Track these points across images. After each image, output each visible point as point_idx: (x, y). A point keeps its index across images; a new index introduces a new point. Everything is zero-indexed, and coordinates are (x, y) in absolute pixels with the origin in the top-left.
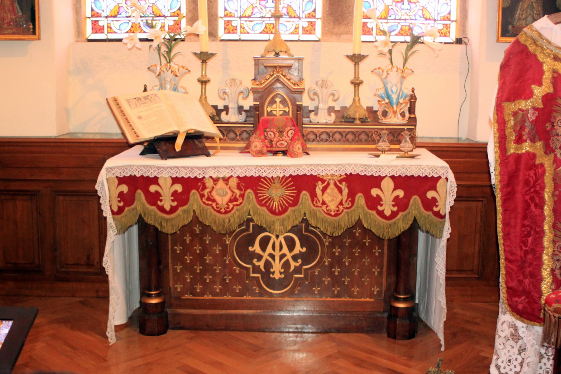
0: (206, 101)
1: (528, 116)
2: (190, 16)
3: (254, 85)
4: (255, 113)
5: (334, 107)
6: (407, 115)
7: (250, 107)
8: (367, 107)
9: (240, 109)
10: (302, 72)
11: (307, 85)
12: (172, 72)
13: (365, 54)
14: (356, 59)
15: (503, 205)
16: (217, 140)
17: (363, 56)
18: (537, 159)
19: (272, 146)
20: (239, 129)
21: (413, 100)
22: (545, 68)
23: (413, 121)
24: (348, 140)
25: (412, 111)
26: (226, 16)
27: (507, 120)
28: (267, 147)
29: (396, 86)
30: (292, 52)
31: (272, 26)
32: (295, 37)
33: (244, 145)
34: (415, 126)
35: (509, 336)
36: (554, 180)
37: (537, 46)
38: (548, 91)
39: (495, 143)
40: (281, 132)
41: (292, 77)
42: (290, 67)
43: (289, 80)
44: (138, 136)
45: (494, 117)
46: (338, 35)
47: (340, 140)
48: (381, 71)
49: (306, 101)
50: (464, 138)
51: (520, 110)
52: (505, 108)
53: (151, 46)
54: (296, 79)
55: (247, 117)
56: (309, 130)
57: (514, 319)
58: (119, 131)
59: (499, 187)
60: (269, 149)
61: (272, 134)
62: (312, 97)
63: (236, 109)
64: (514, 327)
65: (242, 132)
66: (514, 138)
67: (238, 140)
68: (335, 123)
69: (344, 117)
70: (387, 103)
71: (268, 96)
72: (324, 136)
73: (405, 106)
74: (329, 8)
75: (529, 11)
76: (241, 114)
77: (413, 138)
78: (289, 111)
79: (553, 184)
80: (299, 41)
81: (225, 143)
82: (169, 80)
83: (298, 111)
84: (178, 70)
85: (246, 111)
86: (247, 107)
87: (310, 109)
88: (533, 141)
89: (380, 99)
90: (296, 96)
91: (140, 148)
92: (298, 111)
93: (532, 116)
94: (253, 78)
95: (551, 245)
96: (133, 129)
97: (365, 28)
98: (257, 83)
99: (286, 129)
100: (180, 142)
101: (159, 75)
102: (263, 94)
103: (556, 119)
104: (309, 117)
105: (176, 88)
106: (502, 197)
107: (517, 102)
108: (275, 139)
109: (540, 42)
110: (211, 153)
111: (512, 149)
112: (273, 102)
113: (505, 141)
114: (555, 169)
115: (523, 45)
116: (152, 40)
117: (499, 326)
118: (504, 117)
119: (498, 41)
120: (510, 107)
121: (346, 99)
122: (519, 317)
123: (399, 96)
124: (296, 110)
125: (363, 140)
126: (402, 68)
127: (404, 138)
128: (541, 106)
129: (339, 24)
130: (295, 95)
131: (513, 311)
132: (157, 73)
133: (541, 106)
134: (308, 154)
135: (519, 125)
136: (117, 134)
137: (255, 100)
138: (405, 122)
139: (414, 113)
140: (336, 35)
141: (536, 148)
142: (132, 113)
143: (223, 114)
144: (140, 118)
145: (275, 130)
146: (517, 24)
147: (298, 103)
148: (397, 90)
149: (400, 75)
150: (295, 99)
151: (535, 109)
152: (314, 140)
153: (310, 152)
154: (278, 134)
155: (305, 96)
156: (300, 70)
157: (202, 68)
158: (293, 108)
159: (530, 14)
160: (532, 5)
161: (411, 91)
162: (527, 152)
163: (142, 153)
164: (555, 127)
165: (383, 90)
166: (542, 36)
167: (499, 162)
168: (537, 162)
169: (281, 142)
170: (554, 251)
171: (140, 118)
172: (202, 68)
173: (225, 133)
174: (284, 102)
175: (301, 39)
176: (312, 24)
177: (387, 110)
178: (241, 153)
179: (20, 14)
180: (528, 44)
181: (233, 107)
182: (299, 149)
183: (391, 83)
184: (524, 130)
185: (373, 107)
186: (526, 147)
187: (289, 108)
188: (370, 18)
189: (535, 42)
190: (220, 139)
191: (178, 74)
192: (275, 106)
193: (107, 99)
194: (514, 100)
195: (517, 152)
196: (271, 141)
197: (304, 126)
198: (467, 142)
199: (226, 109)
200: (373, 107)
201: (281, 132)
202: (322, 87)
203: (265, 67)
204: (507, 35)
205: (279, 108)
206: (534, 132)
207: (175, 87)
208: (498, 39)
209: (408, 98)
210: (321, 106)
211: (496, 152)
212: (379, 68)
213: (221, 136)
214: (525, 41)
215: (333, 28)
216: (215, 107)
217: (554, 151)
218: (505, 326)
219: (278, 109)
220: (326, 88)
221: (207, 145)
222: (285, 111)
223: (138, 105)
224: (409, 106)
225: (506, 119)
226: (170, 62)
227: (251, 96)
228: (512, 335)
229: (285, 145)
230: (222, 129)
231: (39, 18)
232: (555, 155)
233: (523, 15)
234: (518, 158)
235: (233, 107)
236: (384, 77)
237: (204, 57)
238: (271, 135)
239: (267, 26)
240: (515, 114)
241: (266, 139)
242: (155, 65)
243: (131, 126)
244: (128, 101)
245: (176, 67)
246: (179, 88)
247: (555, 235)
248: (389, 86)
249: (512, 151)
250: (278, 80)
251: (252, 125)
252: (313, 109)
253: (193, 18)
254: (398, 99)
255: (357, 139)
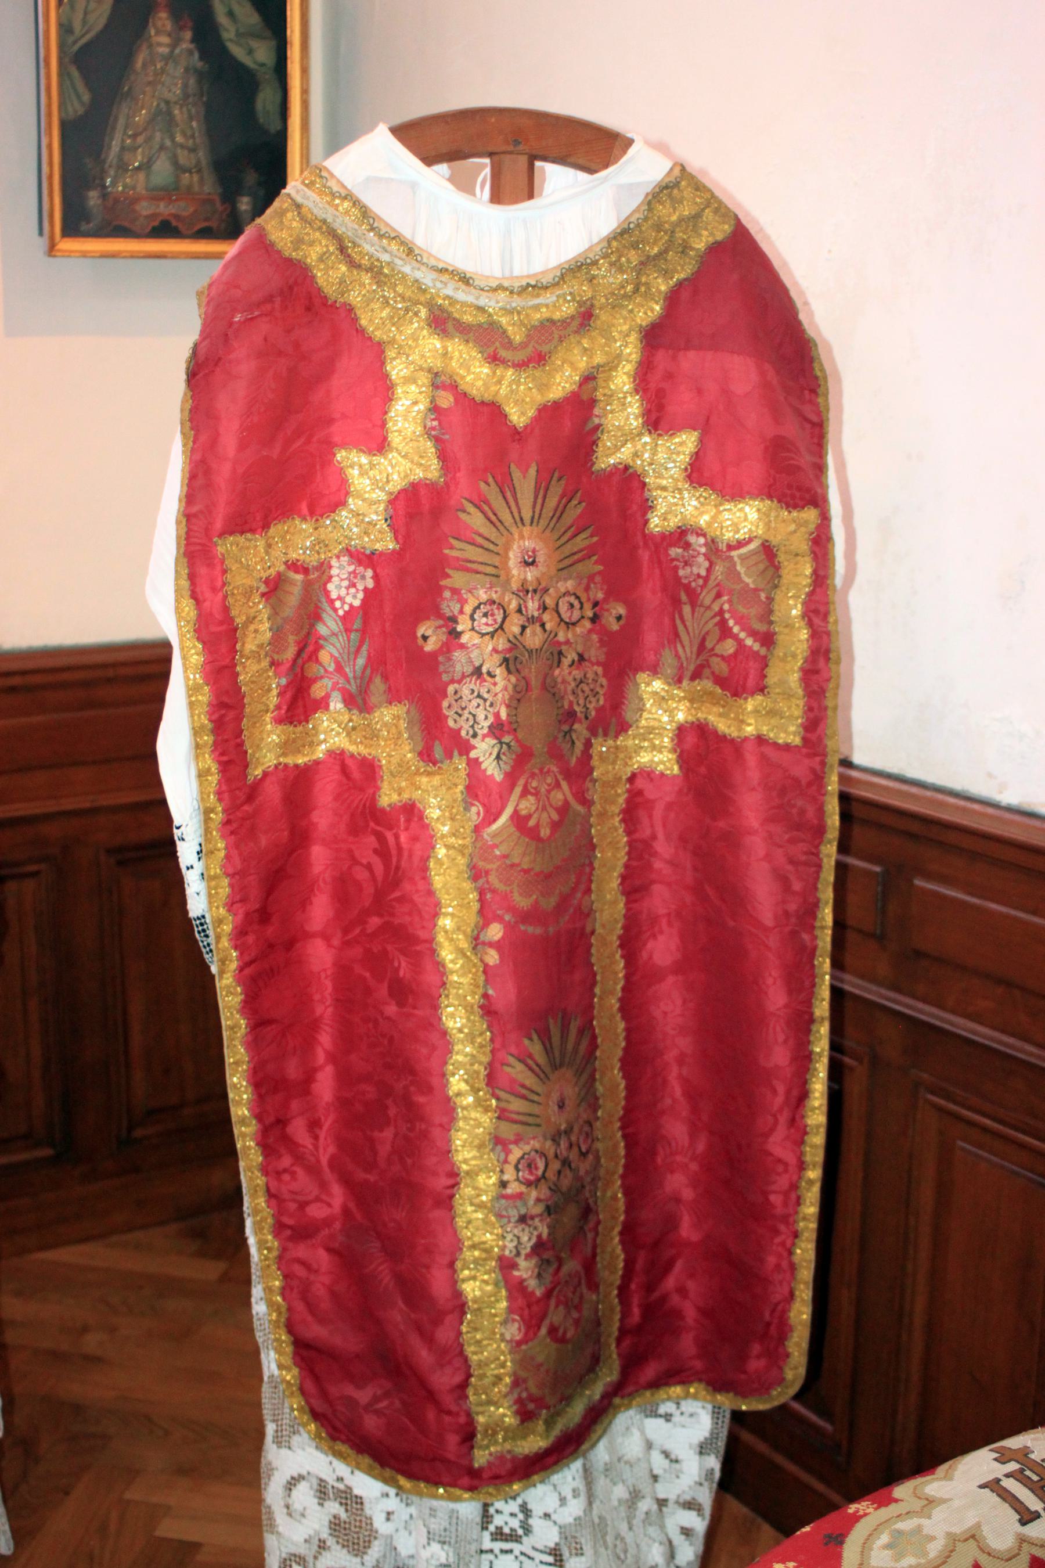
1: (327, 593)
15: (251, 1005)
18: (385, 787)
22: (396, 369)
27: (239, 621)
35: (325, 1534)
36: (476, 874)
37: (353, 264)
38: (419, 474)
39: (196, 732)
45: (178, 610)
51: (294, 566)
52: (230, 564)
57: (342, 1469)
59: (227, 928)
64: (350, 1499)
66: (273, 699)
75: (158, 135)
79: (473, 896)
88: (358, 701)
93: (346, 589)
95: (491, 1158)
103: (463, 602)
106: (241, 969)
109: (370, 246)
111: (268, 747)
113: (239, 718)
114: (477, 829)
115: (289, 261)
117: (273, 1493)
120: (249, 558)
122: (367, 1460)
128: (388, 544)
131: (333, 1438)
133: (388, 544)
135: (291, 639)
141: (375, 735)
151: (363, 558)
159: (162, 148)
160: (169, 113)
162: (338, 757)
164: (464, 639)
166: (376, 218)
167: (218, 817)
168: (388, 797)
170: (503, 1184)
180: (311, 255)
184: (314, 657)
186: (332, 732)
189: (342, 249)
195: (290, 760)
204: (84, 227)
206: (361, 661)
214: (298, 242)
217: (465, 748)
218: (304, 1496)
228: (335, 1525)
232: (474, 764)
234: (298, 782)
240: (274, 587)
247: (502, 1115)
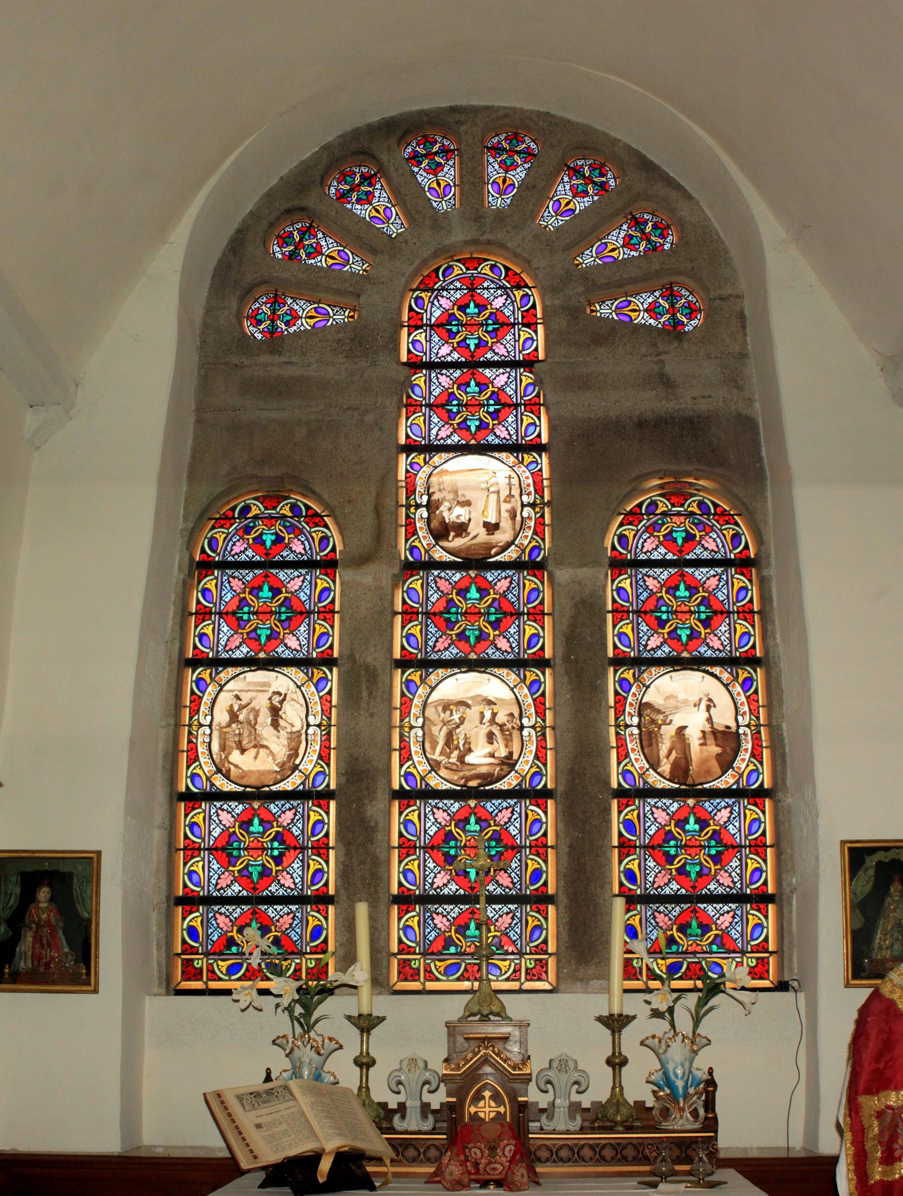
0: (368, 1096)
2: (341, 952)
3: (446, 1069)
4: (451, 1113)
5: (580, 1103)
6: (702, 1112)
7: (442, 1104)
8: (635, 1102)
9: (425, 1108)
10: (526, 1047)
11: (535, 1067)
12: (312, 1048)
13: (631, 1014)
14: (615, 1023)
16: (388, 1162)
17: (627, 1016)
19: (477, 1172)
20: (422, 1142)
21: (711, 1083)
23: (711, 1124)
24: (603, 1158)
25: (710, 1106)
26: (401, 952)
27: (866, 1126)
28: (470, 1173)
29: (682, 1065)
30: (509, 1013)
31: (476, 967)
32: (515, 985)
33: (432, 1170)
34: (716, 1132)
40: (492, 1149)
41: (509, 1055)
42: (505, 1039)
43: (505, 1061)
44: (255, 1157)
46: (585, 980)
47: (591, 1159)
48: (656, 1040)
49: (533, 1095)
50: (798, 1148)
51: (889, 1107)
52: (864, 1105)
53: (277, 1006)
54: (517, 1059)
55: (436, 1121)
56: (540, 1142)
58: (223, 1145)
60: (473, 1177)
61: (478, 1152)
62: (543, 1088)
63: (418, 1109)
65: (428, 1148)
66: (879, 1154)
67: (421, 1161)
68: (582, 1130)
69: (598, 1117)
70: (667, 1095)
71: (471, 1088)
72: (564, 1153)
73: (699, 1098)
74: (570, 936)
76: (427, 1118)
77: (713, 1154)
78: (505, 1112)
80: (520, 991)
81: (400, 1166)
82: (308, 1060)
83: (520, 1111)
84: (323, 1045)
85: (435, 1112)
86: (435, 1106)
87: (541, 1106)
89: (656, 1088)
90: (517, 1086)
91: (262, 1175)
92: (520, 1111)
94: (446, 1056)
96: (248, 1145)
97: (629, 968)
98: (453, 1066)
99: (501, 1144)
100: (325, 1165)
101: (290, 1052)
102: (464, 1085)
104: (539, 1121)
105: (320, 1075)
107: (882, 1094)
108: (484, 1161)
110: (377, 1184)
111: (877, 1173)
112: (478, 1097)
116: (281, 996)
118: (861, 1121)
119: (847, 985)
120: (871, 1104)
121: (599, 1091)
123: (687, 1082)
124: (516, 1109)
125: (630, 1159)
126: (691, 1036)
127: (697, 1154)
129: (586, 962)
130: (515, 1085)
132: (288, 1051)
134: (538, 1183)
136: (220, 1150)
137: (449, 1095)
138: (697, 1126)
139: (714, 1111)
140: (581, 980)
142: (246, 1119)
143: (396, 1118)
144: (259, 1126)
145: (482, 1146)
146: (877, 955)
147: (520, 1099)
148: (684, 1073)
149: (688, 1048)
150: (514, 1090)
152: (547, 1160)
153: (541, 1181)
154: (487, 1152)
155: (532, 1086)
156: (523, 1043)
157: (362, 1041)
158: (511, 1108)
161: (706, 1072)
163: (263, 1186)
165: (660, 1073)
169: (493, 1166)
171: (259, 1126)
172: (362, 1041)
173: (400, 1150)
174: (496, 1097)
175: (524, 987)
176: (543, 964)
177: (668, 1106)
178: (426, 1182)
179: (66, 950)
181: (413, 1105)
182: (522, 1176)
183: (673, 1061)
184: (896, 1141)
185: (644, 1102)
187: (505, 1107)
188: (634, 953)
190: (392, 1161)
191: (322, 1052)
192: (482, 1104)
193: (205, 1095)
194: (877, 1092)
196: (476, 1164)
197: (530, 1136)
198: (803, 1155)
199: (402, 1108)
200: (644, 1102)
201: (492, 1149)
202: (559, 1071)
203: (466, 1039)
204: (862, 975)
205: (489, 1106)
207: (317, 1072)
208: (848, 982)
209: (702, 1086)
210: (558, 1101)
211: (850, 1180)
212: (654, 1037)
213: (394, 1156)
214: (892, 992)
215: (577, 970)
216: (384, 1105)
219: (486, 1109)
220: (566, 1072)
221: (370, 1169)
222: (498, 1113)
223: (256, 1105)
224: (703, 1098)
225: (866, 1123)
226: (308, 1032)
227: (443, 1088)
229: (499, 1171)
230: (394, 1143)
231: (97, 957)
233: (885, 940)
235: (413, 1105)
236: (661, 1051)
237: (366, 1024)
238: (475, 1153)
239: (469, 967)
240: (880, 1115)
241: (468, 1161)
242: (284, 1036)
243: (244, 1139)
244: (240, 1098)
245: (319, 1039)
246: (323, 1074)
248: (670, 1067)
249: (877, 1177)
250: (486, 1061)
251: (445, 1137)
252: (545, 1106)
253: (348, 959)
254: (686, 1087)
255: (619, 1156)
